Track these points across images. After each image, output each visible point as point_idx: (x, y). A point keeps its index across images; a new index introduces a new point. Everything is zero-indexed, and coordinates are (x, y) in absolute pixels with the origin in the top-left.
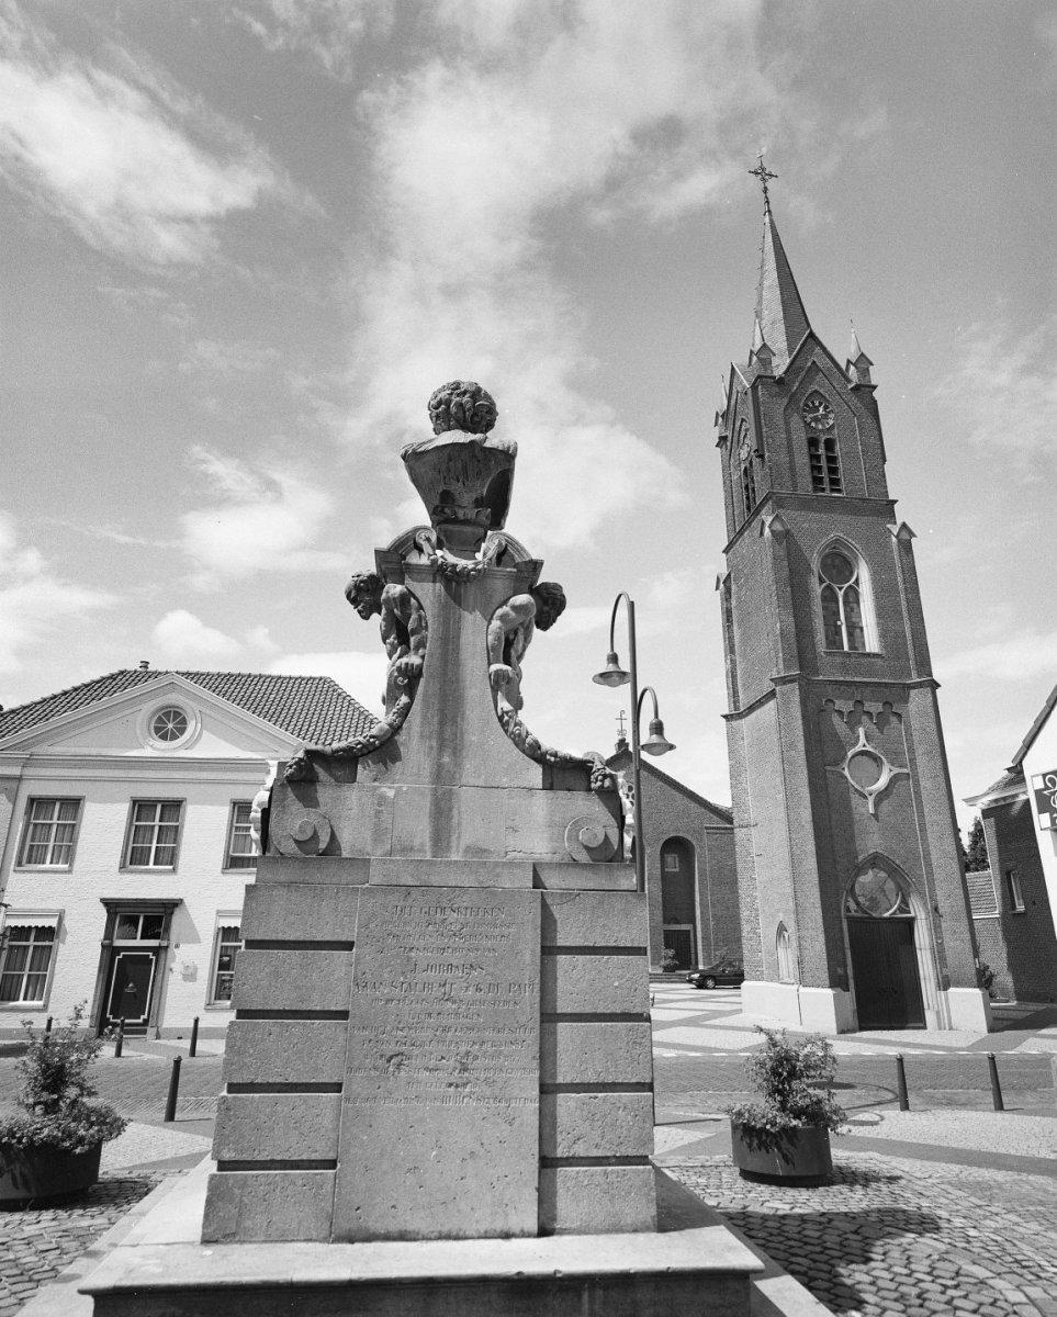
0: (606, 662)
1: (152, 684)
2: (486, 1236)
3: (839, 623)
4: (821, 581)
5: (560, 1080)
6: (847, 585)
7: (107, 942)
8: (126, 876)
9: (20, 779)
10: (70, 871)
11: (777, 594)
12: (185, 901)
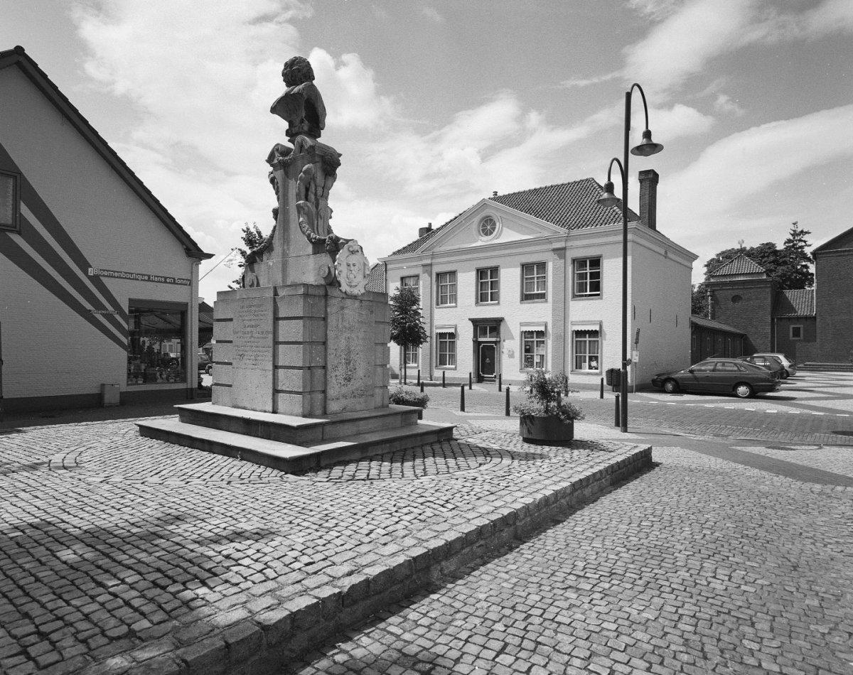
0: (642, 138)
2: (261, 411)
5: (279, 365)
10: (456, 307)
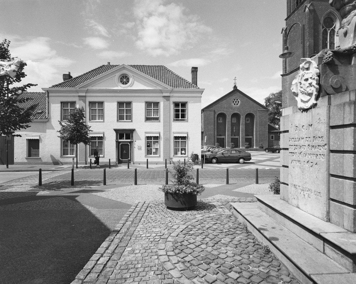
1: (114, 69)
3: (327, 42)
4: (323, 28)
6: (331, 28)
7: (117, 140)
8: (119, 123)
9: (85, 96)
10: (104, 122)
11: (309, 32)
12: (136, 129)
